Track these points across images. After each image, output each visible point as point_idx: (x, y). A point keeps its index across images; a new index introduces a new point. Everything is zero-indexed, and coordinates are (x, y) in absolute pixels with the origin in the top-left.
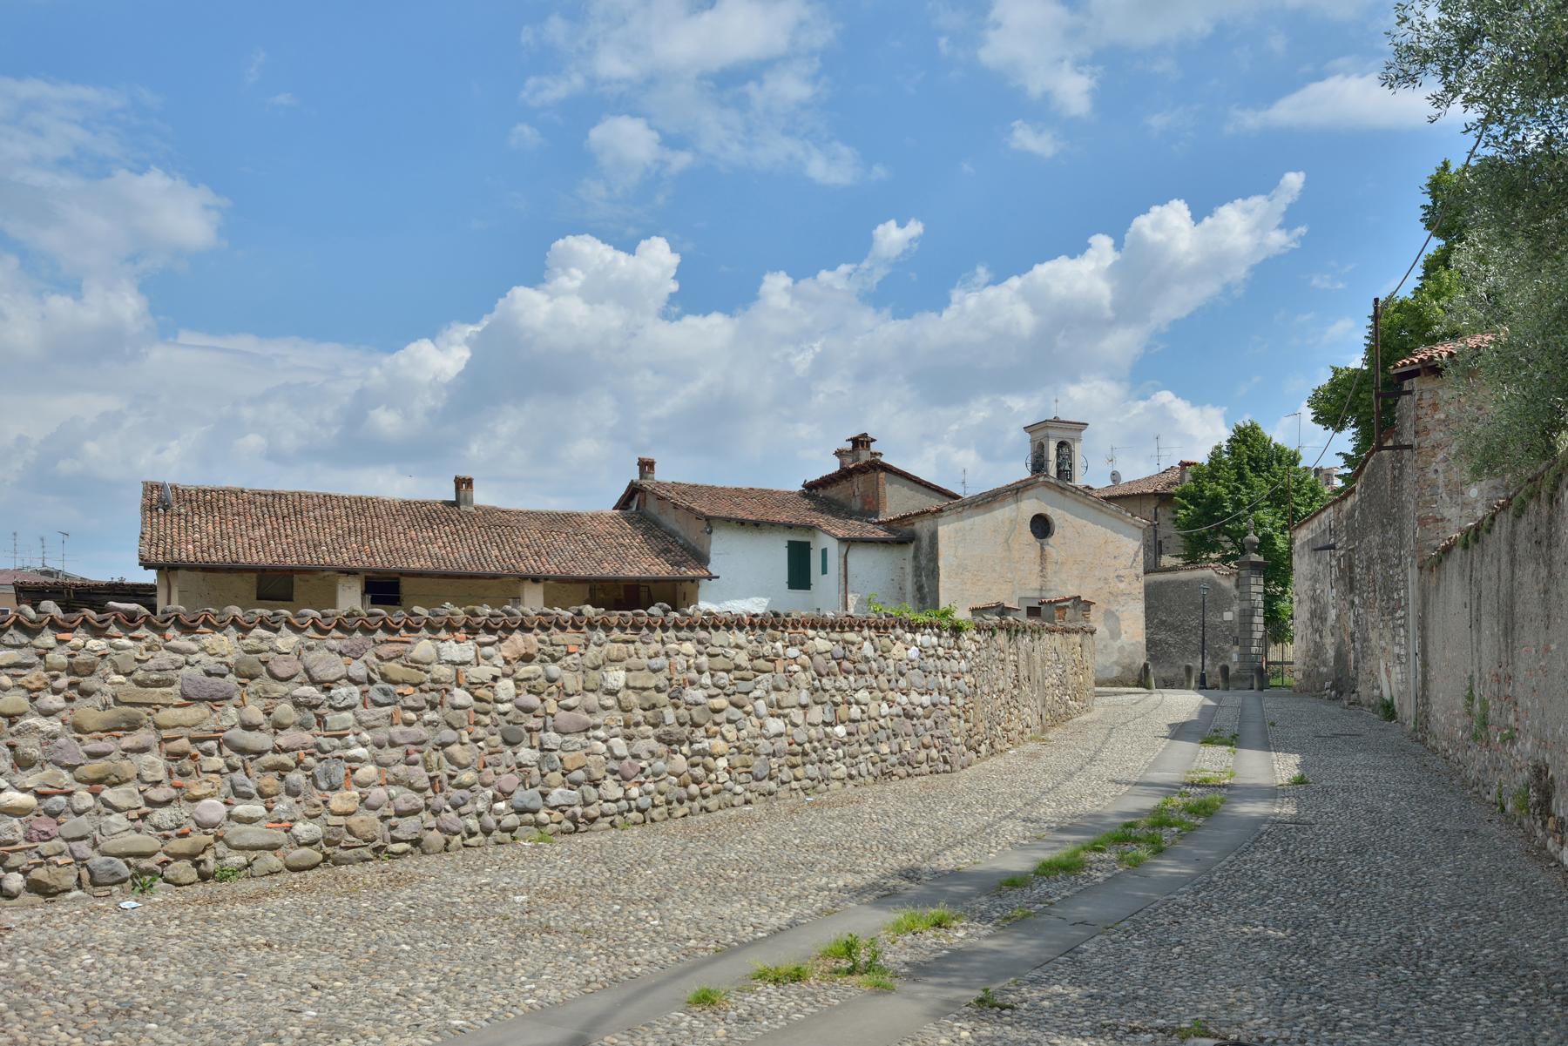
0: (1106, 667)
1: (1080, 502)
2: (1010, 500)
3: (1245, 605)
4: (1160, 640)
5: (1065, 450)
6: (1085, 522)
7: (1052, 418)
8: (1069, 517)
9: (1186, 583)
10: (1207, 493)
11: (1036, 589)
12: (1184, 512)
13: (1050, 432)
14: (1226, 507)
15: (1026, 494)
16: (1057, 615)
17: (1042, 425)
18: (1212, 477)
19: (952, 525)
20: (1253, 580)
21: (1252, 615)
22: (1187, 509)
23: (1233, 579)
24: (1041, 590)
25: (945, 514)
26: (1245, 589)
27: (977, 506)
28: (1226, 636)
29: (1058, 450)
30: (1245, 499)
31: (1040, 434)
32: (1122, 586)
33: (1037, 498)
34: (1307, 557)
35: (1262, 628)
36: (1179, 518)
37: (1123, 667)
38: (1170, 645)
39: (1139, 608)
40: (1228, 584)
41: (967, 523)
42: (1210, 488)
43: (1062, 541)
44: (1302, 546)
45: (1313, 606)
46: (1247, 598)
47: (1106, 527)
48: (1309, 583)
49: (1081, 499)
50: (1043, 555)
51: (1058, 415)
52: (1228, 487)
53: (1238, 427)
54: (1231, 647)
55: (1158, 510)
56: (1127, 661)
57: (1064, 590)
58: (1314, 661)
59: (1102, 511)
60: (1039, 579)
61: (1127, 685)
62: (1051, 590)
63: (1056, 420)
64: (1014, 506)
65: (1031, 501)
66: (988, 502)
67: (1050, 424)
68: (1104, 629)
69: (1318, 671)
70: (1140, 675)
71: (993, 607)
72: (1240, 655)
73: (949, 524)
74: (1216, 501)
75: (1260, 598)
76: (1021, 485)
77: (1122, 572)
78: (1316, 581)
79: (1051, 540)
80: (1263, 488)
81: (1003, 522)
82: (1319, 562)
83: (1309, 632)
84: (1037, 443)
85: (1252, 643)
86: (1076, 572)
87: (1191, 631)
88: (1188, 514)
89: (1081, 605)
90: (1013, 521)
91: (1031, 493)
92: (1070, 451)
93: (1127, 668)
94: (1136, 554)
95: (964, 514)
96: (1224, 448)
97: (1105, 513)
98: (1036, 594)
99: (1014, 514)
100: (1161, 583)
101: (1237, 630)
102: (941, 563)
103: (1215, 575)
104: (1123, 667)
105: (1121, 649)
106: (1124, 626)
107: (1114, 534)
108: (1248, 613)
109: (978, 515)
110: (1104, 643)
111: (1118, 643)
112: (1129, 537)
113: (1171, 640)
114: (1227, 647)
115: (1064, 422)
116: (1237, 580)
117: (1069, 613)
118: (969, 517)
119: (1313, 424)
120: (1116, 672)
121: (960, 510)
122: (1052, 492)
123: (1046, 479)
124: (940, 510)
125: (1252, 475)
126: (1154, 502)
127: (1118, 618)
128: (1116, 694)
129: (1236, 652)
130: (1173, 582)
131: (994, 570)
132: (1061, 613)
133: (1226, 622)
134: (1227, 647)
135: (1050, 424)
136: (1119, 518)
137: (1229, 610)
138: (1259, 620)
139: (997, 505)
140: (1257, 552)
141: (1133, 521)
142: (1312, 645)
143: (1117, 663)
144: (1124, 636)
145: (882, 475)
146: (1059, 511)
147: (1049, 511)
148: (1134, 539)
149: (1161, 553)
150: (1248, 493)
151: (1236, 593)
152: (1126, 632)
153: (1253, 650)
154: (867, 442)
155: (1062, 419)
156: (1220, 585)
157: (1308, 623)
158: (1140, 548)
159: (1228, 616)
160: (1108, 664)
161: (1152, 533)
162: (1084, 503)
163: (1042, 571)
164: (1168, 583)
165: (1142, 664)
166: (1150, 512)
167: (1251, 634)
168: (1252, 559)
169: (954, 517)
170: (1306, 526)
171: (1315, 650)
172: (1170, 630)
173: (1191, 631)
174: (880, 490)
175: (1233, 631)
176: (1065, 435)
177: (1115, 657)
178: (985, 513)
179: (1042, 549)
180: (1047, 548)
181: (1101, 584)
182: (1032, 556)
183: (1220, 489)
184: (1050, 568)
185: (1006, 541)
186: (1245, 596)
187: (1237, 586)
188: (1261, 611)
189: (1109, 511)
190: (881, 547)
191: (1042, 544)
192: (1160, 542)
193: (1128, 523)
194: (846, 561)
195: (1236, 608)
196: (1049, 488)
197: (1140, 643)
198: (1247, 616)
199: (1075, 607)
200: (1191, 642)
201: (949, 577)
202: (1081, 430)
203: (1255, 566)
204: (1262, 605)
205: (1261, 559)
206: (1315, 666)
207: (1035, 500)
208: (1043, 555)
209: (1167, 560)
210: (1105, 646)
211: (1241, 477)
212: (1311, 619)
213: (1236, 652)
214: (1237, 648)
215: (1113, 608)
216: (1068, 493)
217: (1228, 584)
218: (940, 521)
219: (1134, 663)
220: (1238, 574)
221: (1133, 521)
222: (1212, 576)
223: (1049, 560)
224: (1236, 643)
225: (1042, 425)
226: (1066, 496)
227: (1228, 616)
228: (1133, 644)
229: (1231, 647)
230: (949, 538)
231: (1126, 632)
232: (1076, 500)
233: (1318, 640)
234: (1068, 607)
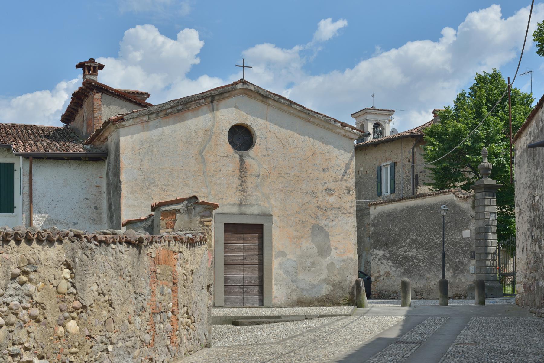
0: (314, 286)
1: (284, 111)
2: (205, 108)
3: (481, 223)
4: (411, 257)
5: (379, 129)
6: (290, 132)
7: (370, 107)
8: (272, 127)
9: (431, 207)
10: (450, 130)
11: (234, 205)
12: (431, 148)
13: (369, 116)
14: (466, 141)
15: (223, 103)
16: (163, 223)
17: (363, 112)
18: (456, 118)
19: (135, 136)
20: (487, 201)
21: (487, 232)
22: (433, 145)
23: (470, 201)
24: (241, 205)
25: (127, 123)
26: (480, 209)
27: (166, 115)
28: (465, 252)
29: (374, 129)
30: (482, 134)
31: (361, 119)
32: (331, 199)
33: (236, 107)
34: (526, 164)
35: (495, 243)
36: (427, 154)
37: (333, 285)
38: (419, 261)
39: (351, 222)
40: (466, 205)
41: (154, 134)
42: (451, 126)
43: (265, 153)
44: (522, 155)
45: (532, 215)
46: (482, 217)
47: (314, 138)
48: (527, 192)
49: (285, 108)
50: (243, 168)
51: (374, 106)
52: (467, 124)
53: (479, 76)
54: (469, 261)
55: (415, 150)
56: (338, 278)
57: (266, 205)
58: (534, 274)
59: (309, 121)
60: (239, 193)
61: (336, 304)
62: (251, 205)
63: (373, 109)
64: (209, 115)
65: (230, 109)
66: (179, 111)
67: (368, 111)
68: (312, 246)
69: (538, 285)
70: (352, 293)
71: (141, 221)
72: (477, 267)
73: (133, 134)
74: (457, 136)
75: (493, 216)
76: (216, 92)
77: (331, 186)
78: (535, 188)
79: (251, 152)
80: (499, 124)
81: (196, 132)
82: (537, 166)
83: (529, 242)
84: (360, 125)
85: (487, 256)
86: (281, 186)
87: (436, 248)
88: (435, 150)
89: (199, 209)
90: (209, 133)
91: (232, 100)
92: (382, 129)
93: (337, 286)
94: (348, 166)
95: (151, 123)
96: (467, 95)
97: (313, 123)
98: (235, 210)
99: (210, 124)
100: (412, 208)
101: (474, 246)
102: (123, 177)
103: (455, 199)
104: (333, 285)
105: (331, 266)
106: (334, 241)
107: (323, 146)
108: (483, 230)
109: (166, 125)
110: (311, 260)
111: (328, 260)
112: (339, 148)
113: (420, 257)
114: (465, 261)
115: (378, 110)
116: (474, 202)
117: (181, 220)
118: (157, 127)
119: (538, 55)
120: (325, 290)
121: (145, 118)
122: (253, 101)
123: (245, 86)
124: (121, 119)
125: (488, 114)
126: (412, 143)
127: (327, 235)
128: (307, 317)
129: (473, 265)
130: (422, 206)
131: (187, 185)
132: (170, 220)
133: (464, 239)
134: (465, 261)
135: (368, 111)
136: (328, 129)
137: (467, 229)
138: (493, 236)
139: (190, 114)
140: (492, 177)
141: (343, 132)
142: (531, 256)
143: (326, 281)
144: (333, 253)
145: (98, 96)
146: (262, 121)
147: (250, 121)
148: (345, 151)
149: (417, 184)
150: (486, 129)
151: (473, 213)
152: (336, 248)
153: (488, 262)
154: (95, 67)
155: (377, 108)
156: (459, 207)
157: (528, 233)
158: (351, 160)
159: (466, 234)
160: (316, 282)
161: (410, 169)
162: (289, 113)
163: (241, 185)
164: (418, 207)
165: (354, 282)
166: (409, 152)
167: (486, 249)
168: (486, 183)
169: (140, 126)
170: (525, 133)
171: (535, 262)
172: (419, 248)
173: (436, 248)
174: (96, 110)
175: (470, 246)
176: (379, 119)
177: (324, 274)
178: (175, 123)
179: (242, 161)
180: (247, 160)
181: (308, 198)
182: (231, 169)
183: (460, 125)
184: (251, 182)
185: (201, 153)
186: (480, 215)
187: (474, 207)
188: (494, 229)
189: (317, 121)
190: (74, 165)
191: (241, 156)
192: (417, 176)
193: (338, 134)
194: (31, 180)
195: (473, 227)
196: (250, 96)
197: (351, 259)
198: (482, 233)
199: (188, 211)
200: (436, 257)
201: (133, 192)
202: (390, 115)
203: (488, 189)
204: (495, 223)
205: (494, 182)
206: (535, 279)
207: (234, 109)
208: (243, 168)
209: (423, 189)
210: (313, 264)
211: (479, 115)
212: (531, 230)
213: (473, 265)
214: (474, 262)
215: (322, 223)
216: (270, 102)
217: (466, 205)
218: (122, 131)
219: (345, 280)
220: (474, 196)
221: (343, 132)
222: (452, 200)
223: (249, 173)
224: (473, 257)
225: (363, 112)
226: (269, 105)
227: (466, 234)
228: (344, 261)
229: (469, 261)
230: (133, 149)
231: (336, 248)
232: (280, 109)
233: (538, 250)
234: (178, 211)
